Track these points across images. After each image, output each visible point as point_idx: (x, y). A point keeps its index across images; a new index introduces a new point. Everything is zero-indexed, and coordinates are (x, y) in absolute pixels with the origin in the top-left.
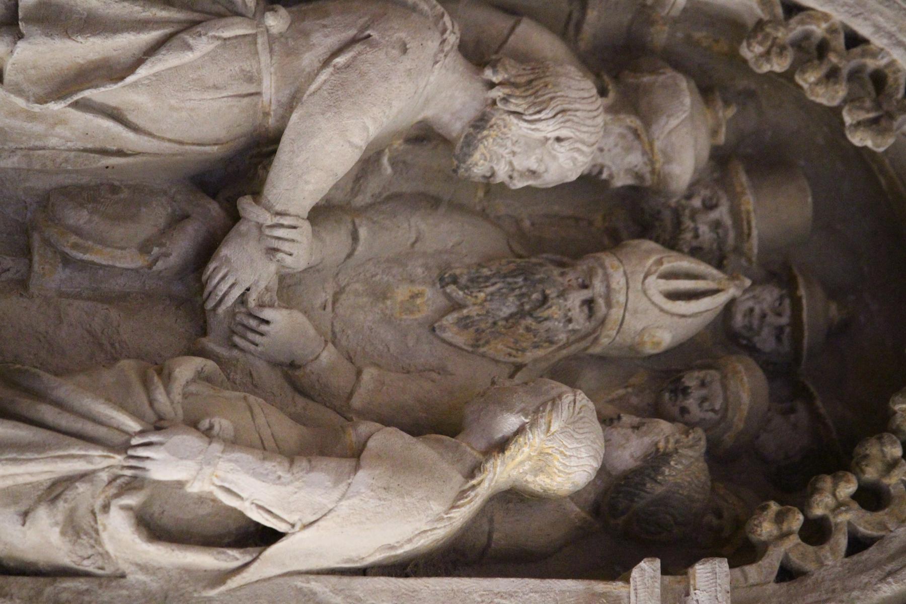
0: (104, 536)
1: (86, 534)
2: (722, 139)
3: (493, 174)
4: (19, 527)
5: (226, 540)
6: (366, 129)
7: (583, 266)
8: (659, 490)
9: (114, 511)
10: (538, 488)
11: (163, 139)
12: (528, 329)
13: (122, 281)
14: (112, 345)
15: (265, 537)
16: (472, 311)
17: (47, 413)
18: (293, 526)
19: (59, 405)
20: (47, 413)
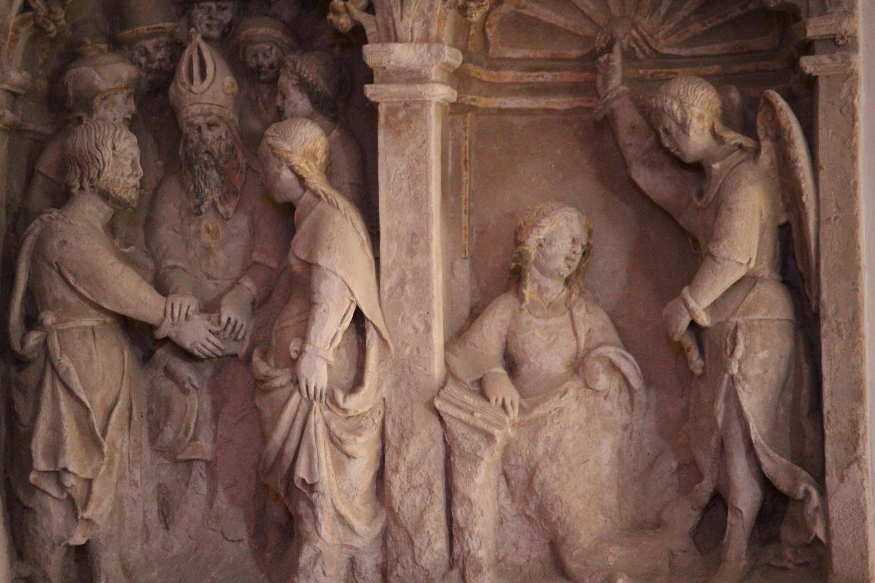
0: (361, 411)
1: (359, 422)
2: (104, 46)
3: (135, 186)
4: (357, 461)
5: (361, 340)
6: (112, 264)
7: (186, 130)
8: (321, 82)
9: (346, 406)
10: (324, 157)
11: (121, 384)
12: (226, 162)
13: (205, 406)
14: (244, 410)
15: (359, 317)
16: (216, 196)
17: (291, 447)
18: (352, 302)
19: (285, 440)
20: (291, 447)
